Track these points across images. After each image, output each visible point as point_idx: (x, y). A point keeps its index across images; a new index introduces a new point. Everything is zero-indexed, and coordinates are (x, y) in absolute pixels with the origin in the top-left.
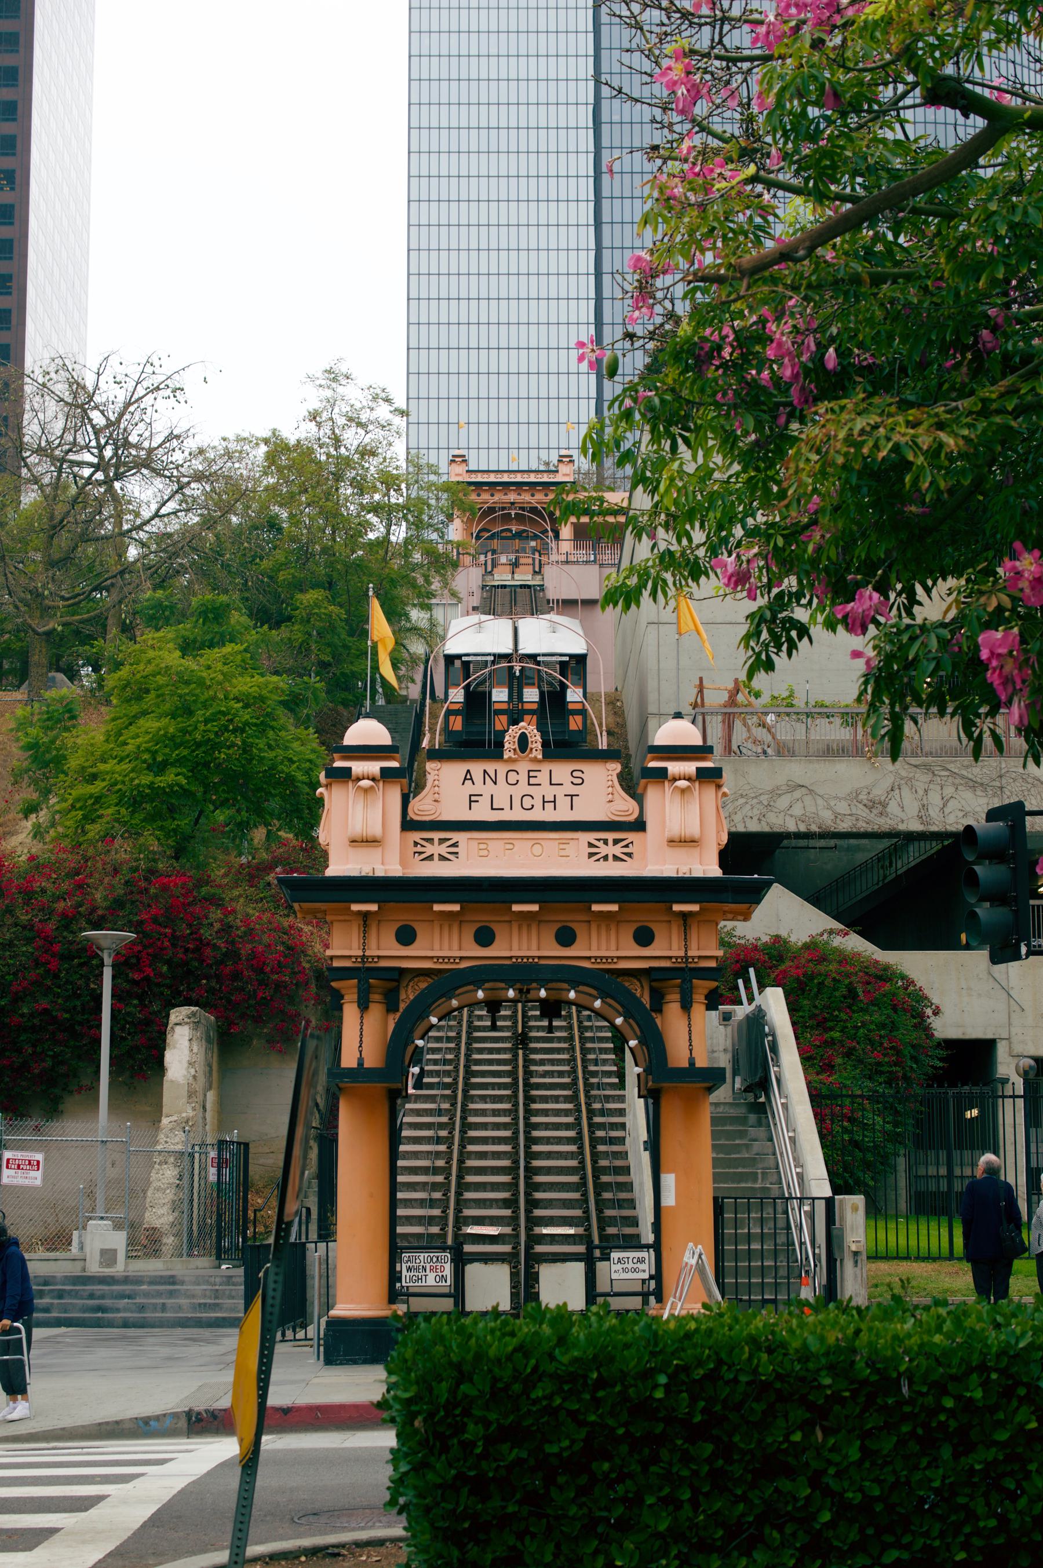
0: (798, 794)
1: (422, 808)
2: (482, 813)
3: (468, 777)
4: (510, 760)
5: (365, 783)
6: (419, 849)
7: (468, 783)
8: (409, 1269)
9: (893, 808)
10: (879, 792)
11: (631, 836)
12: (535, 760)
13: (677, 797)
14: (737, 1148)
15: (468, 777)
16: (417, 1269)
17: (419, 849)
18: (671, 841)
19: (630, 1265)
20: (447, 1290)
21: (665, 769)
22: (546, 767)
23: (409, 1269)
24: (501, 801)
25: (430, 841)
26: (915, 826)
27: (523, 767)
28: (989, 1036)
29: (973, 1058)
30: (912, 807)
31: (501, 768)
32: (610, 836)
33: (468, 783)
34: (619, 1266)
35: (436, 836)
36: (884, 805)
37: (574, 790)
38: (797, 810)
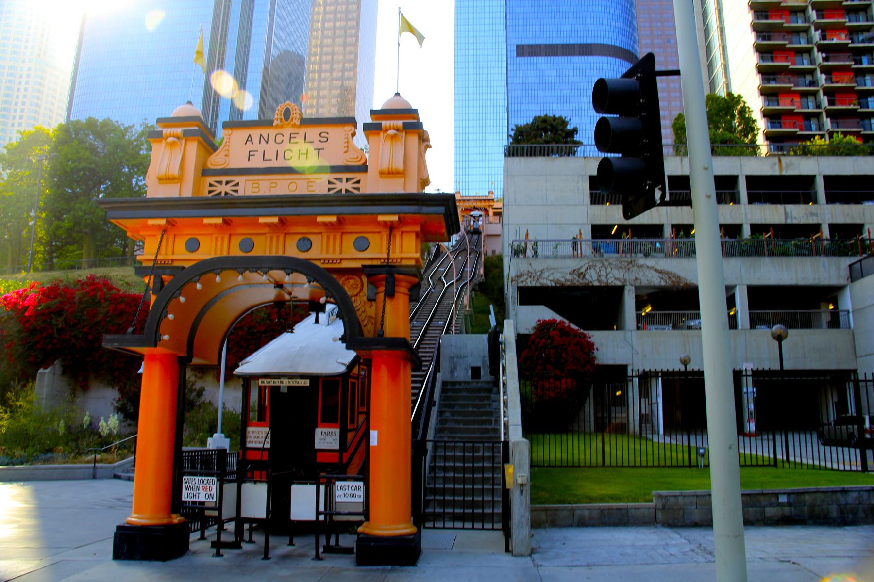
0: (551, 272)
1: (216, 161)
2: (257, 163)
3: (249, 139)
4: (277, 126)
5: (170, 139)
6: (212, 188)
7: (249, 143)
8: (187, 488)
9: (587, 277)
10: (583, 270)
11: (358, 176)
12: (294, 125)
13: (389, 142)
14: (484, 406)
15: (249, 139)
16: (193, 488)
17: (212, 188)
18: (382, 173)
19: (350, 492)
20: (213, 505)
21: (381, 124)
22: (302, 131)
23: (187, 488)
24: (271, 155)
25: (220, 182)
26: (596, 284)
27: (287, 131)
28: (625, 363)
29: (619, 373)
30: (595, 277)
31: (272, 132)
32: (344, 176)
33: (249, 143)
34: (342, 492)
35: (224, 179)
36: (584, 276)
37: (321, 145)
38: (551, 278)
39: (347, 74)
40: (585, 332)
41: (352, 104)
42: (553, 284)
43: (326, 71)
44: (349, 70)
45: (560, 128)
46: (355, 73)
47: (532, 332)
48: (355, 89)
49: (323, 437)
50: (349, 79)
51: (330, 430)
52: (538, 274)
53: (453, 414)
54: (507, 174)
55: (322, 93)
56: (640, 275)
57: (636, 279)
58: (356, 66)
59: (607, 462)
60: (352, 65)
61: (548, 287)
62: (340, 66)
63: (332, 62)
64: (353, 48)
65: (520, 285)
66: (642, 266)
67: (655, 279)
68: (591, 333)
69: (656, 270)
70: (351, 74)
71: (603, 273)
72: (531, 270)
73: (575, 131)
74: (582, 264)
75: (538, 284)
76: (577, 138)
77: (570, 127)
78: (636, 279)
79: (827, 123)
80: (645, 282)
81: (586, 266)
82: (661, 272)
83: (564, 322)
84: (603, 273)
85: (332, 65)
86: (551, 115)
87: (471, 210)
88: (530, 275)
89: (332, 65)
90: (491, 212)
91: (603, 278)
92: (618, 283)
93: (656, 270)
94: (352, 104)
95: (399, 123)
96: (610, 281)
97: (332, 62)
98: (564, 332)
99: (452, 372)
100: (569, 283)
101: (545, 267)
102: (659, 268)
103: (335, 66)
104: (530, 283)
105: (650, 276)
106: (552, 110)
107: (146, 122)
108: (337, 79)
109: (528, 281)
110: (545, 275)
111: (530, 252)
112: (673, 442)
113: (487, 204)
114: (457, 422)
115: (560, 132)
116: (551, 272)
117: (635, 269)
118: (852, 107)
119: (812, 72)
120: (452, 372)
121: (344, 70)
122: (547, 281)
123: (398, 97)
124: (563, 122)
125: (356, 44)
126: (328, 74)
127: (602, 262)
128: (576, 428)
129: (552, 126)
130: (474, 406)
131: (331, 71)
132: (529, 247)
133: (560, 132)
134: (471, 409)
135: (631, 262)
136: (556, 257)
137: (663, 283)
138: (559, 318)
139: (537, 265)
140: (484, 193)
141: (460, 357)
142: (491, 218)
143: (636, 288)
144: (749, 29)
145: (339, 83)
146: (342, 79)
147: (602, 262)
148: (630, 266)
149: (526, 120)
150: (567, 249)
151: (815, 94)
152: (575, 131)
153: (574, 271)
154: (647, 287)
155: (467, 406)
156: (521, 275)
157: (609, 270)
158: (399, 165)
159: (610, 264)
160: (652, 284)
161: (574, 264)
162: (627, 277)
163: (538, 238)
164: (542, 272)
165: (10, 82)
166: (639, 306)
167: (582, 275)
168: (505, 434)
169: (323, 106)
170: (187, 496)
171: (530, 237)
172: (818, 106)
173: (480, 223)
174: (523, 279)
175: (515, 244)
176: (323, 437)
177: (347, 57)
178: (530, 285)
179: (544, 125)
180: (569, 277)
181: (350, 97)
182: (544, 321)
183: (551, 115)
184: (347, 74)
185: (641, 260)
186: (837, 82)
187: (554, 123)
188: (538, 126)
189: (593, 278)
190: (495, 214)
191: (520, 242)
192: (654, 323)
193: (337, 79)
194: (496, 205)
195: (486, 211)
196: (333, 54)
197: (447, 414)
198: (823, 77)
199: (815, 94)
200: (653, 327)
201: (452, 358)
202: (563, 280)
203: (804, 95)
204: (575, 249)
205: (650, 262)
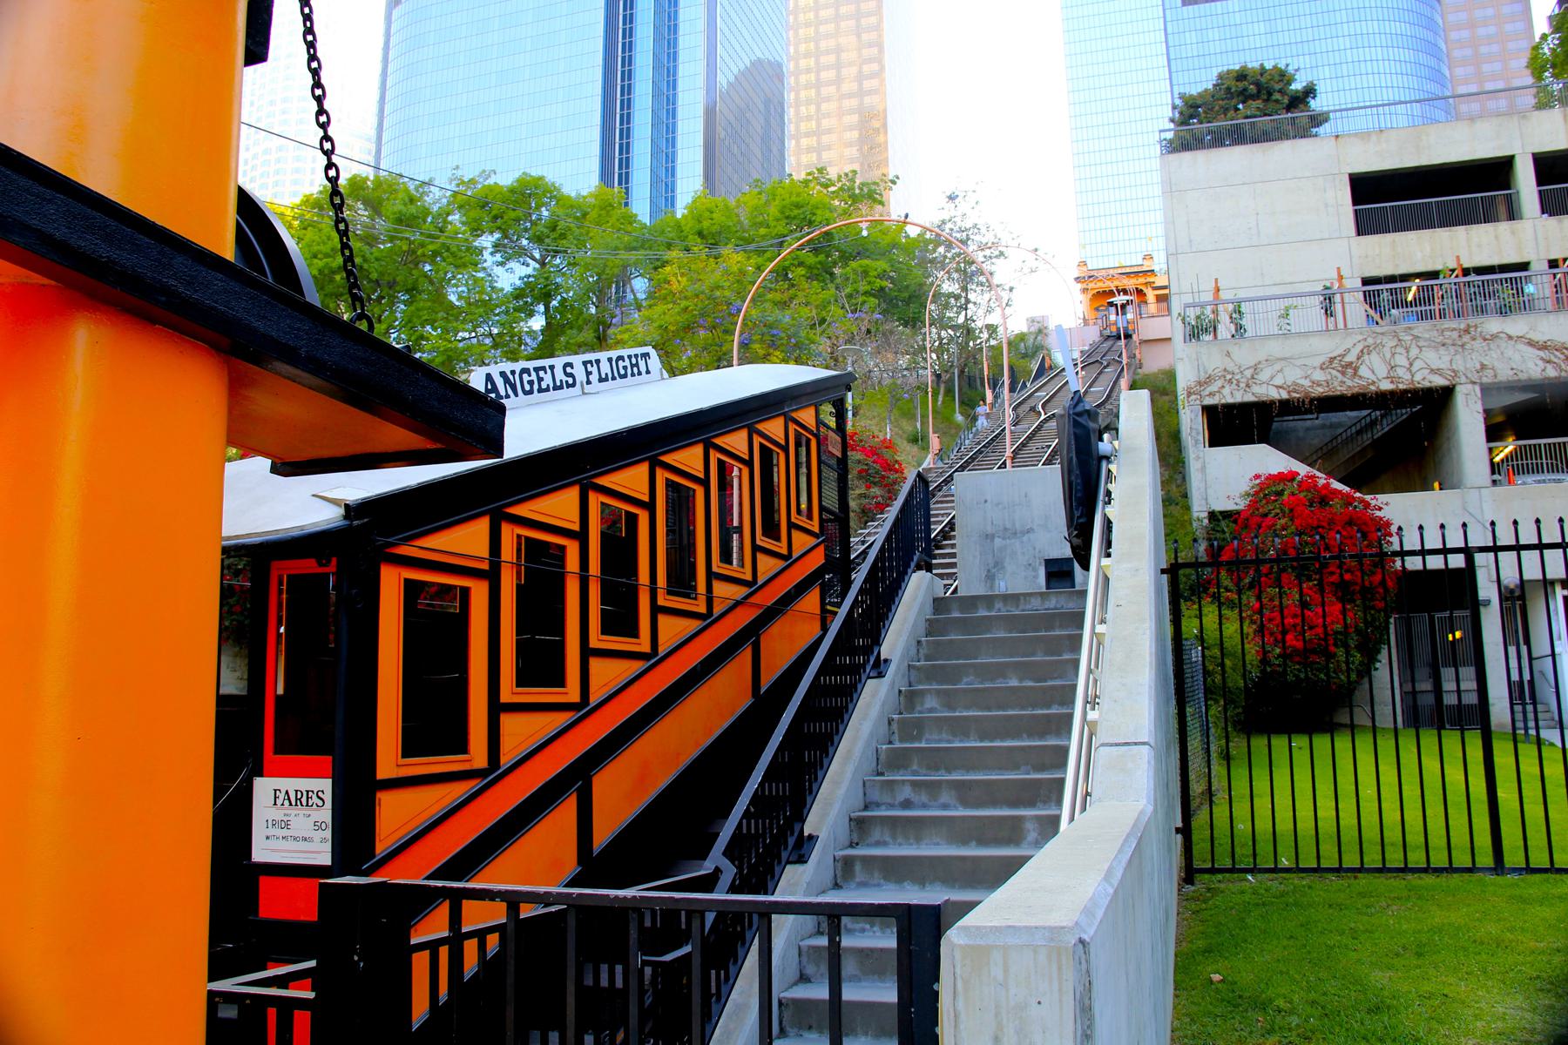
0: (1277, 367)
9: (1364, 371)
10: (1351, 358)
26: (1386, 386)
29: (1454, 589)
30: (1382, 371)
36: (1356, 370)
38: (1278, 381)
39: (867, 84)
40: (1368, 497)
41: (881, 138)
42: (1285, 395)
43: (829, 83)
44: (872, 76)
45: (1277, 87)
46: (882, 81)
47: (1241, 505)
48: (885, 111)
49: (278, 814)
50: (870, 93)
51: (304, 784)
52: (1248, 373)
53: (949, 699)
54: (1171, 190)
55: (825, 123)
56: (1493, 358)
57: (1483, 367)
58: (882, 68)
59: (1513, 857)
60: (875, 67)
61: (1272, 402)
62: (854, 70)
63: (838, 66)
64: (873, 36)
65: (1209, 401)
66: (1494, 337)
67: (1531, 365)
68: (1382, 498)
69: (1531, 343)
70: (874, 83)
71: (1401, 360)
72: (1231, 367)
73: (1310, 91)
74: (1348, 344)
75: (1249, 398)
76: (1316, 105)
77: (1297, 86)
78: (1483, 367)
80: (1505, 374)
81: (1359, 347)
82: (1544, 347)
83: (1314, 476)
84: (1401, 360)
85: (839, 72)
86: (1253, 64)
87: (1111, 294)
88: (1228, 377)
89: (839, 72)
90: (1151, 295)
91: (1400, 372)
92: (1439, 381)
93: (1531, 343)
94: (881, 138)
96: (1418, 378)
97: (838, 66)
98: (1324, 497)
99: (990, 578)
100: (1321, 390)
101: (1261, 356)
102: (1538, 337)
103: (844, 71)
104: (1232, 395)
105: (1517, 357)
106: (1258, 55)
107: (459, 173)
108: (850, 96)
109: (1226, 391)
110: (1264, 376)
111: (1225, 329)
113: (1142, 280)
114: (959, 727)
115: (1277, 96)
116: (1277, 367)
117: (1478, 344)
120: (990, 578)
121: (860, 78)
122: (1269, 390)
124: (1283, 77)
125: (878, 28)
126: (832, 89)
127: (1396, 335)
128: (1362, 718)
129: (1257, 84)
130: (1024, 670)
131: (838, 81)
132: (1224, 318)
133: (1277, 96)
134: (1014, 683)
135: (1467, 331)
136: (1287, 335)
137: (1551, 372)
138: (1302, 469)
139: (1244, 355)
140: (1134, 260)
141: (1011, 533)
142: (1152, 307)
143: (1486, 390)
145: (854, 102)
146: (861, 93)
147: (1396, 335)
148: (1466, 338)
149: (1201, 81)
150: (1311, 314)
152: (1310, 91)
153: (1332, 359)
154: (1511, 387)
155: (1000, 671)
156: (1209, 380)
157: (1414, 352)
159: (1416, 338)
160: (1523, 376)
161: (1330, 346)
162: (1459, 364)
163: (1242, 294)
164: (1256, 368)
165: (297, 171)
166: (1494, 433)
167: (1351, 368)
169: (829, 148)
171: (1223, 295)
173: (1130, 316)
174: (1213, 388)
175: (1192, 314)
176: (278, 814)
177: (865, 52)
178: (1230, 400)
179: (1241, 85)
180: (1319, 376)
181: (876, 124)
182: (1270, 477)
183: (1256, 65)
184: (867, 84)
185: (1493, 325)
187: (1263, 80)
188: (1229, 89)
189: (1377, 375)
190: (1160, 299)
191: (1202, 306)
192: (1538, 469)
193: (850, 96)
194: (1160, 281)
195: (1140, 292)
196: (838, 50)
197: (930, 702)
200: (1530, 479)
201: (990, 537)
202: (1306, 383)
204: (1329, 312)
205: (1517, 325)
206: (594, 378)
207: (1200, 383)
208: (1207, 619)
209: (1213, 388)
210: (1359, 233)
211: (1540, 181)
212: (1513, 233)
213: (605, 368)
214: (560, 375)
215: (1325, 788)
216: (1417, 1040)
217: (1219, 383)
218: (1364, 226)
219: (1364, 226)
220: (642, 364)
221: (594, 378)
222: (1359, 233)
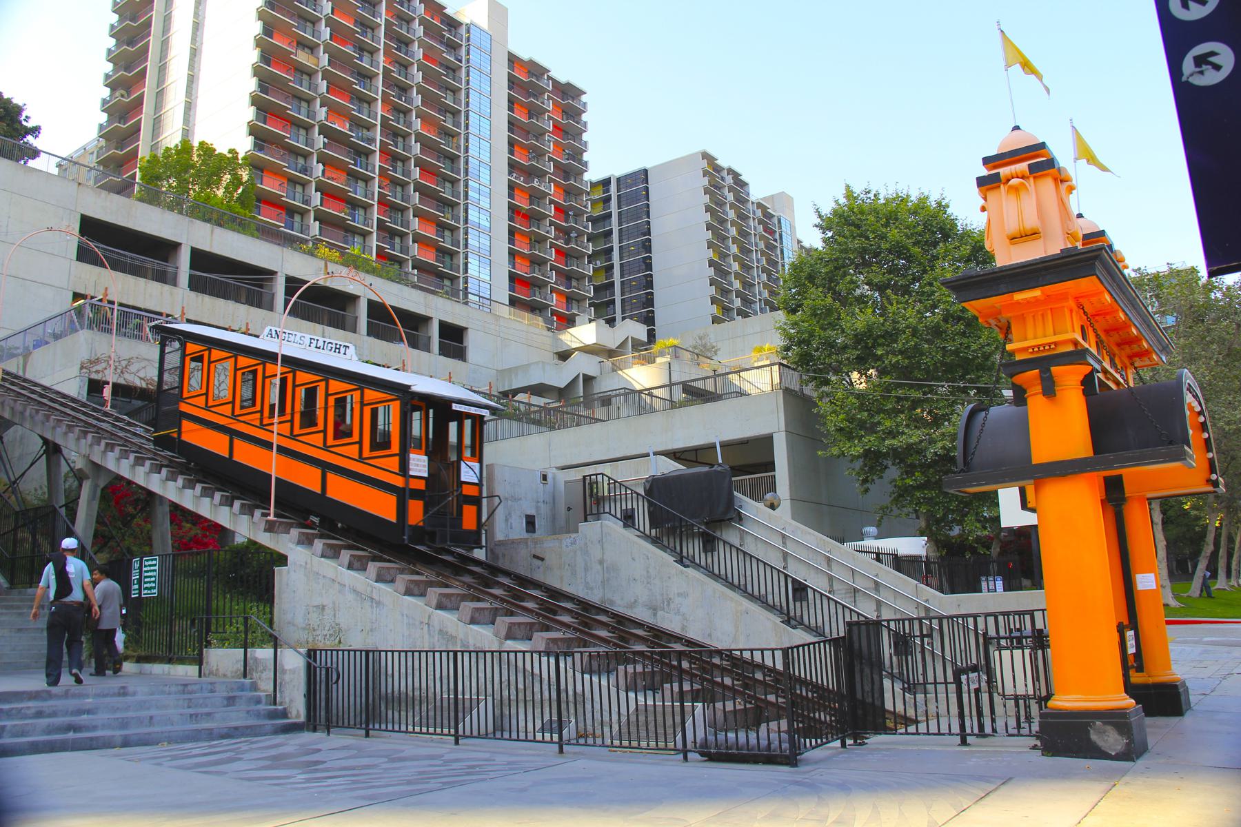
0: (143, 364)
38: (142, 374)
42: (144, 385)
52: (124, 363)
61: (135, 388)
65: (95, 376)
79: (315, 227)
95: (1023, 167)
110: (133, 368)
112: (650, 702)
116: (143, 364)
118: (342, 215)
119: (306, 155)
123: (1017, 132)
144: (249, 71)
151: (304, 184)
156: (97, 361)
158: (1031, 222)
164: (129, 360)
168: (1036, 659)
170: (1133, 680)
172: (307, 202)
174: (99, 367)
186: (333, 179)
198: (321, 166)
199: (304, 184)
203: (293, 181)
206: (314, 345)
207: (90, 362)
208: (994, 514)
209: (99, 367)
210: (78, 259)
211: (192, 267)
212: (171, 294)
213: (320, 344)
214: (298, 339)
215: (522, 716)
216: (1230, 353)
217: (104, 365)
218: (84, 255)
219: (84, 255)
220: (342, 350)
221: (314, 345)
222: (78, 259)
